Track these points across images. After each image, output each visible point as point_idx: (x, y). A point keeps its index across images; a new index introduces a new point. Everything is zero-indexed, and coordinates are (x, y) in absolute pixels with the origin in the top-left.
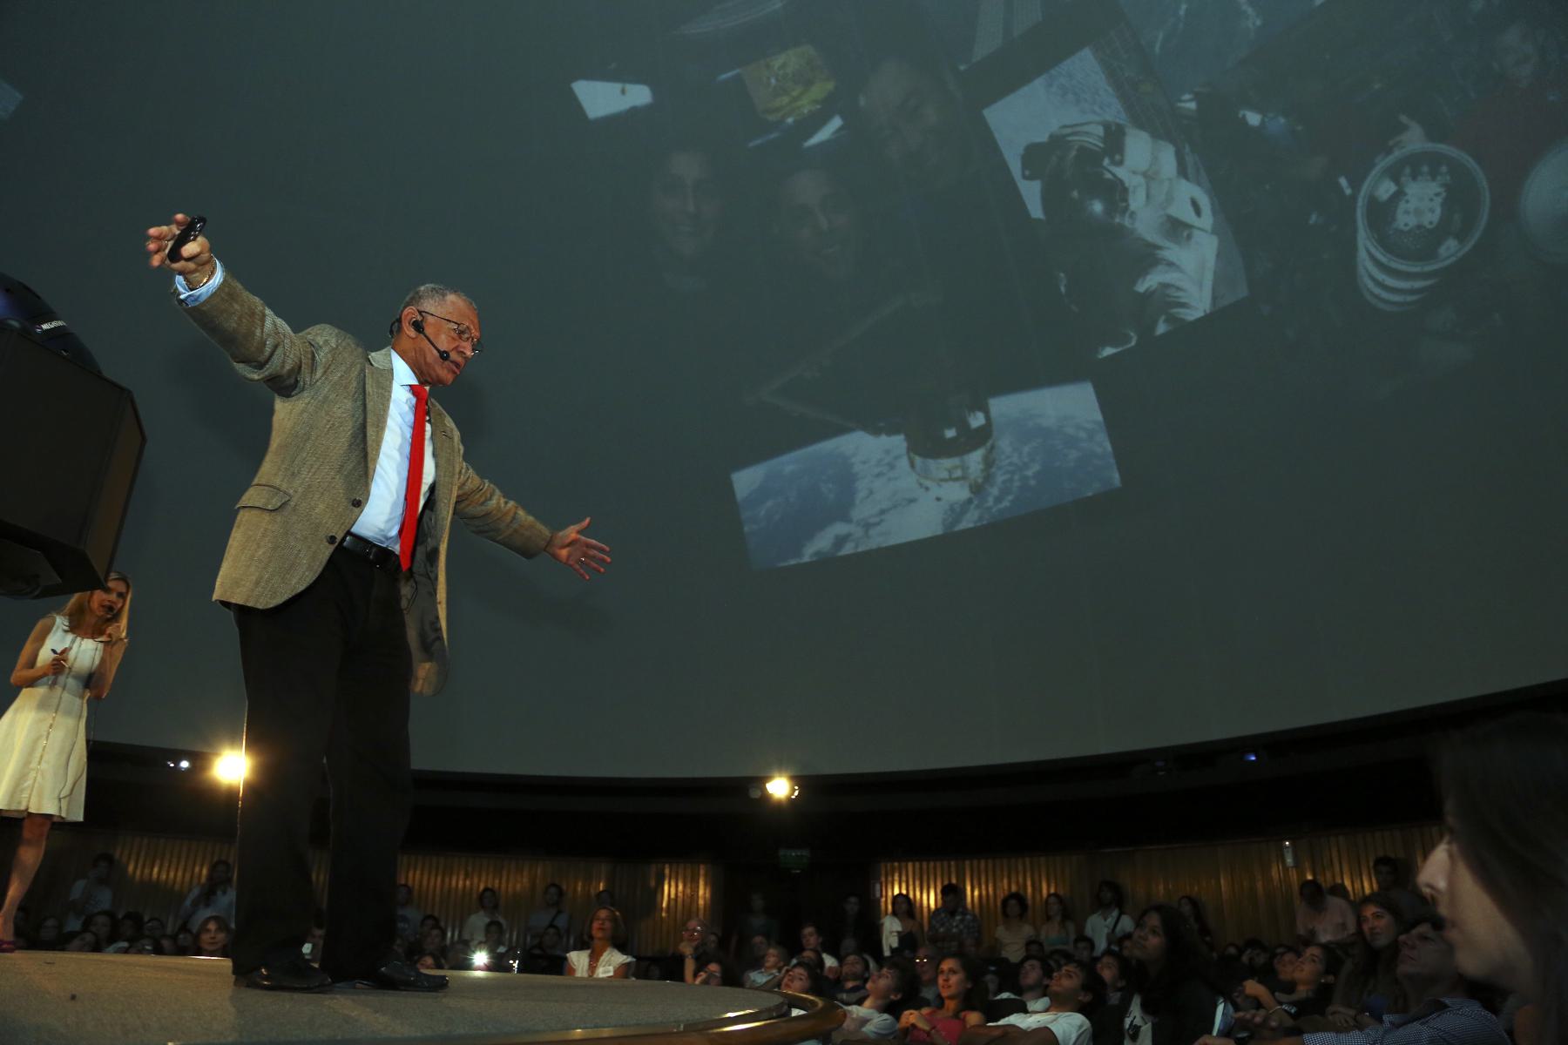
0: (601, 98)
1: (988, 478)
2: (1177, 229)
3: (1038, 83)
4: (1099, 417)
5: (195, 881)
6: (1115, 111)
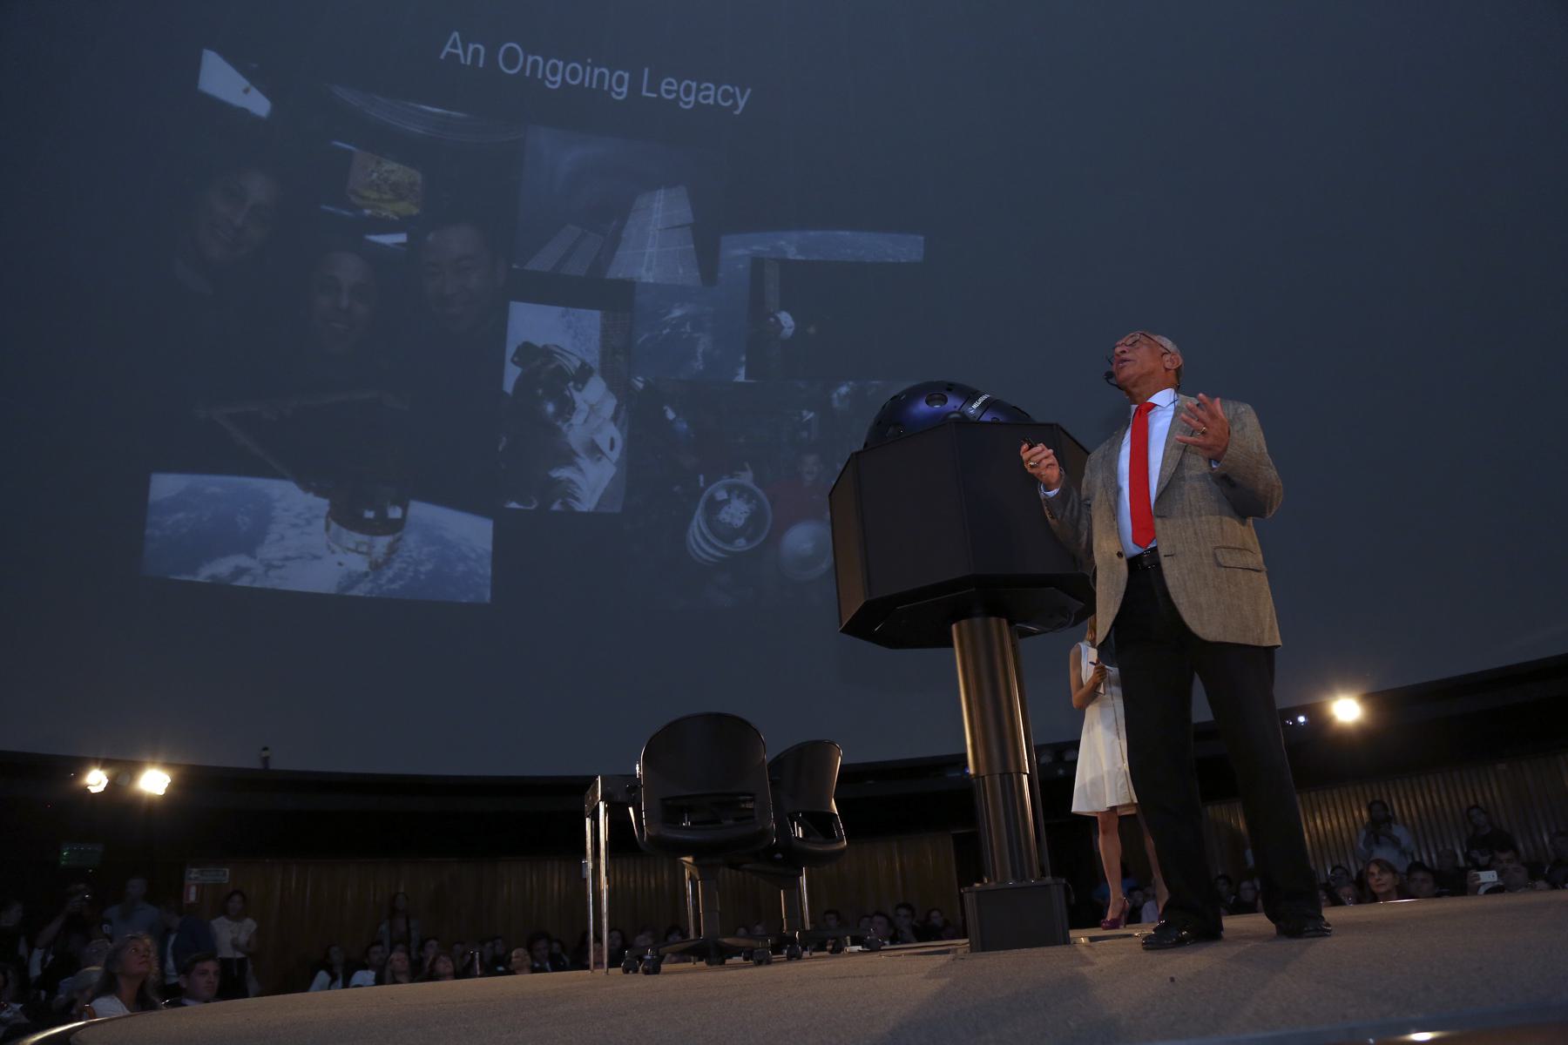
0: (220, 79)
1: (388, 561)
2: (594, 450)
3: (557, 310)
4: (489, 547)
5: (1360, 826)
6: (593, 359)
